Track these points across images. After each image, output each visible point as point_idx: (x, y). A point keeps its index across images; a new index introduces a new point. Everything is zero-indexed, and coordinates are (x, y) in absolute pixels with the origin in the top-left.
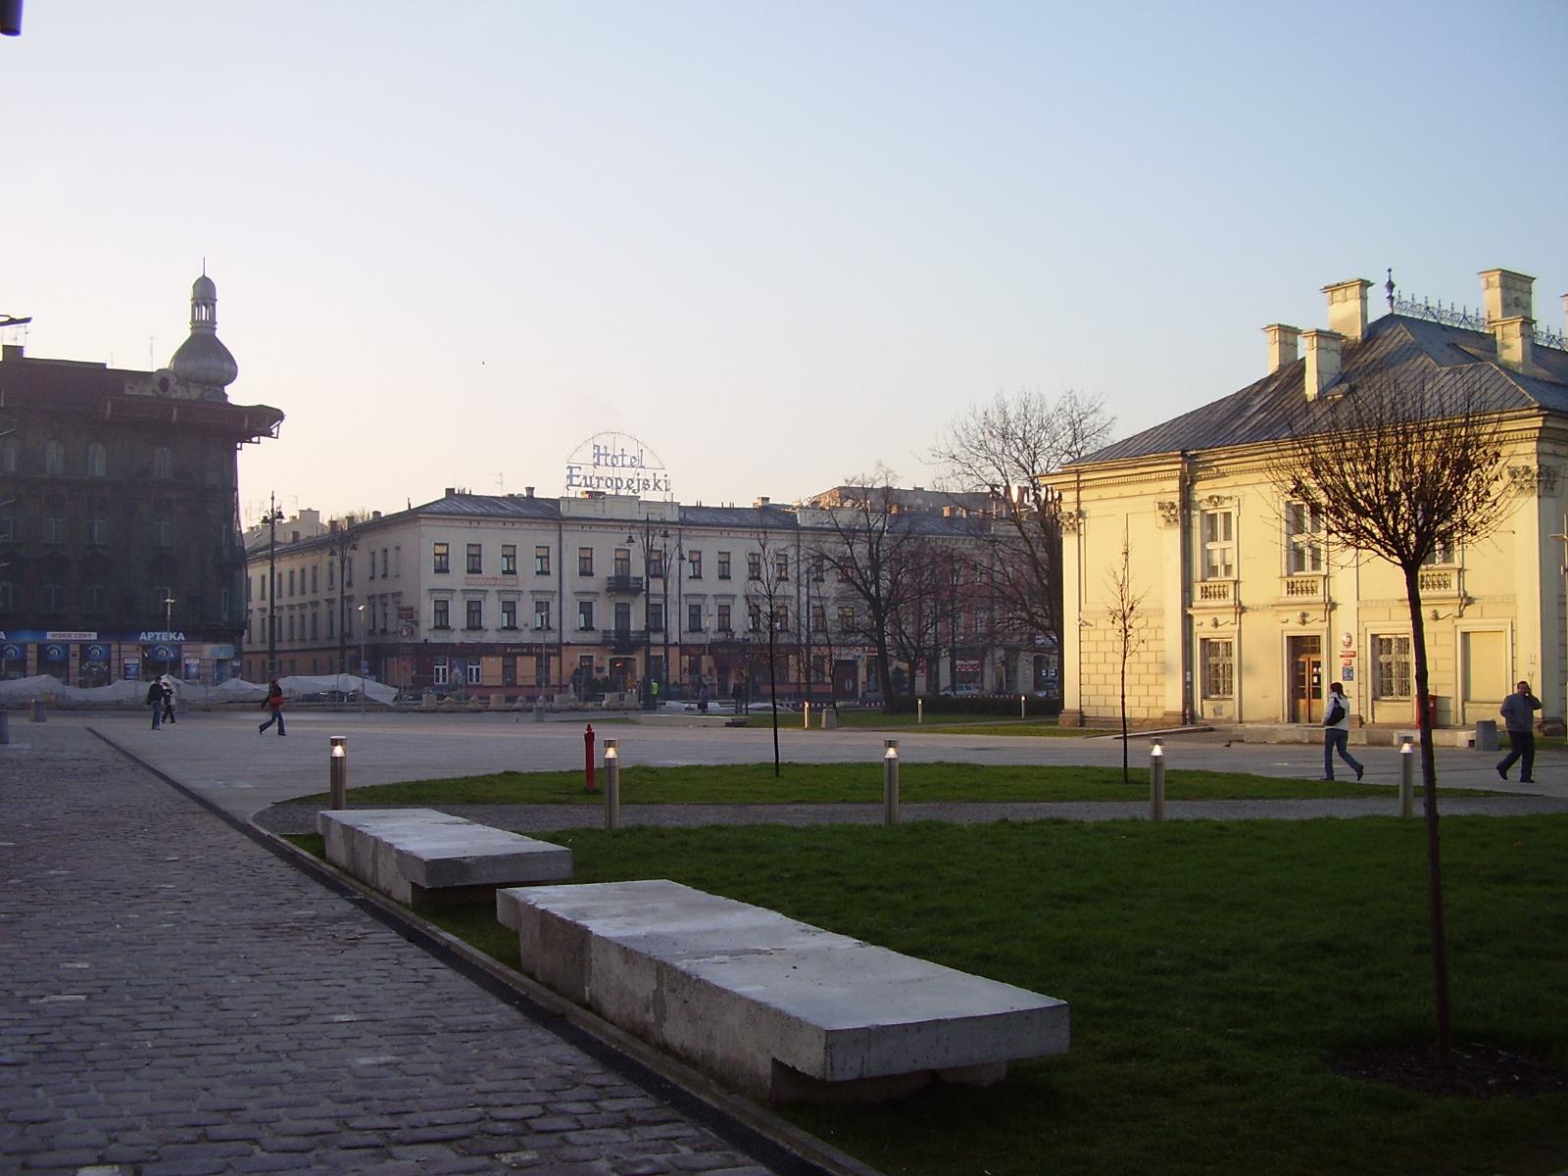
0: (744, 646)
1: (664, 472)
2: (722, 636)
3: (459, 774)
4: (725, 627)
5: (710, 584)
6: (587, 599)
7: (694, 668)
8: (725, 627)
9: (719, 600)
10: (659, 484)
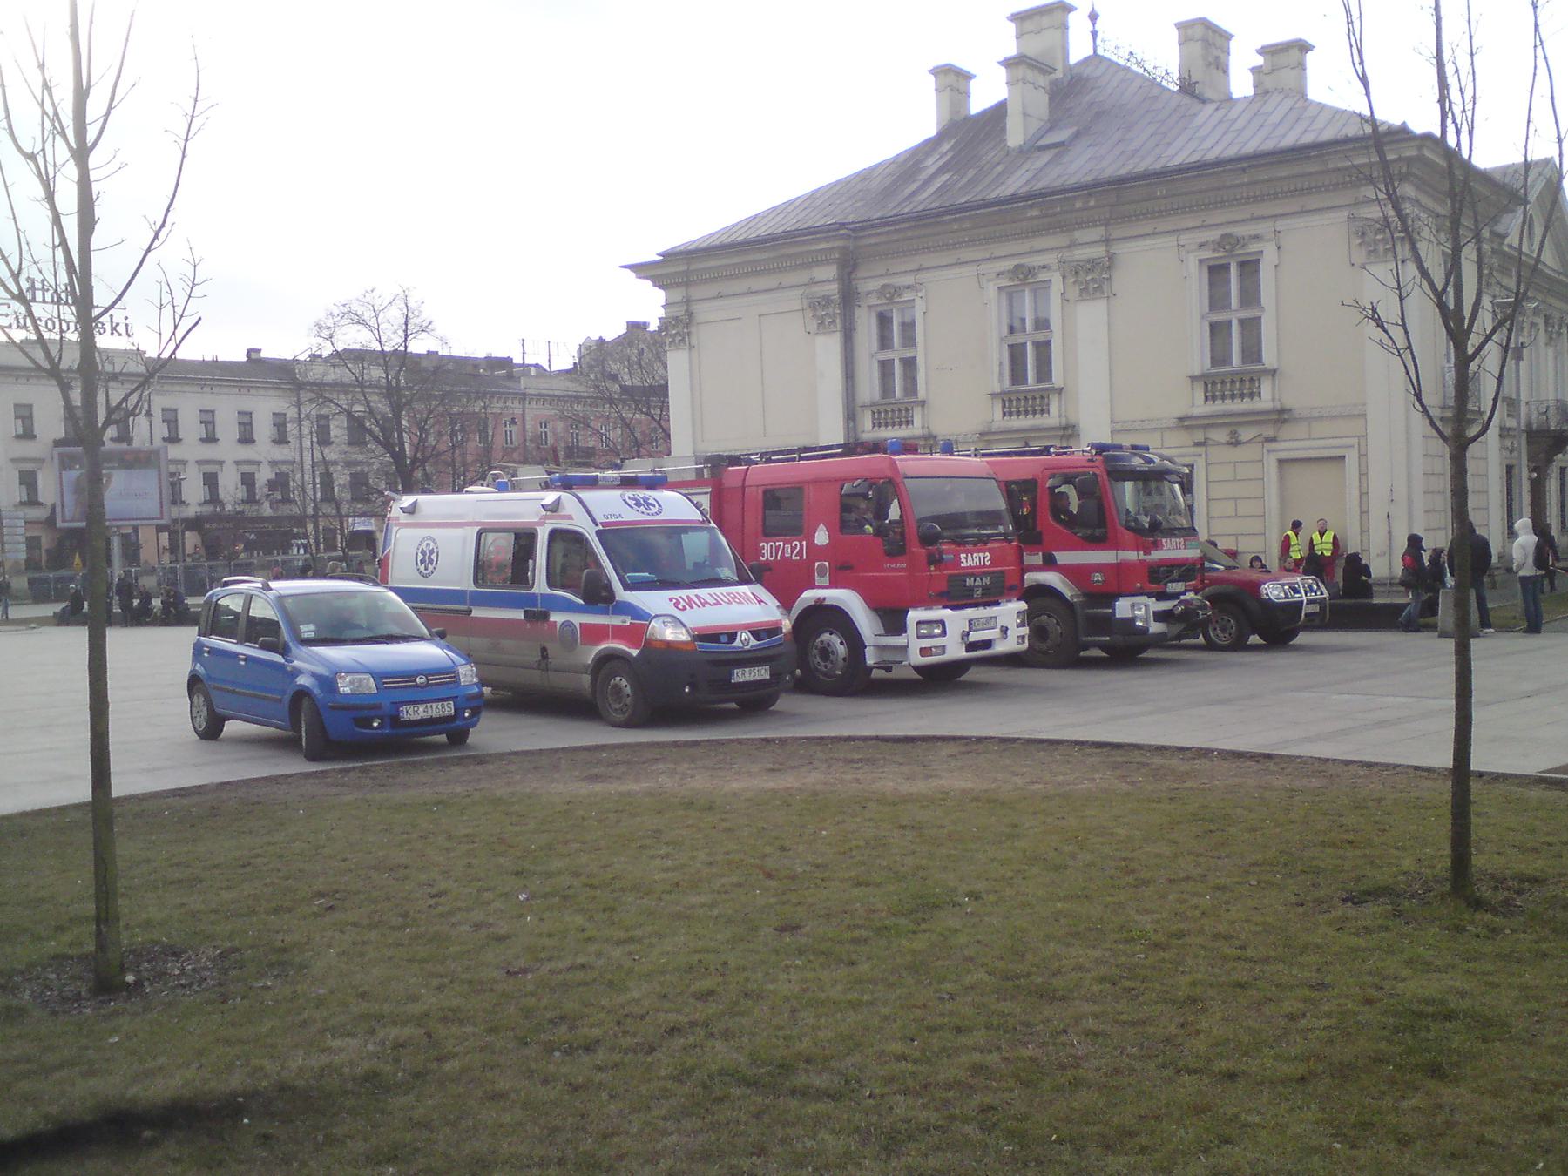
0: (238, 519)
1: (124, 314)
2: (208, 509)
3: (1064, 671)
4: (214, 499)
5: (228, 449)
6: (29, 467)
7: (175, 547)
8: (214, 499)
9: (202, 467)
10: (118, 328)
